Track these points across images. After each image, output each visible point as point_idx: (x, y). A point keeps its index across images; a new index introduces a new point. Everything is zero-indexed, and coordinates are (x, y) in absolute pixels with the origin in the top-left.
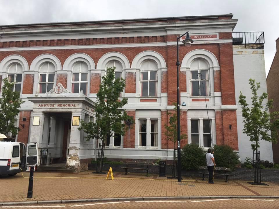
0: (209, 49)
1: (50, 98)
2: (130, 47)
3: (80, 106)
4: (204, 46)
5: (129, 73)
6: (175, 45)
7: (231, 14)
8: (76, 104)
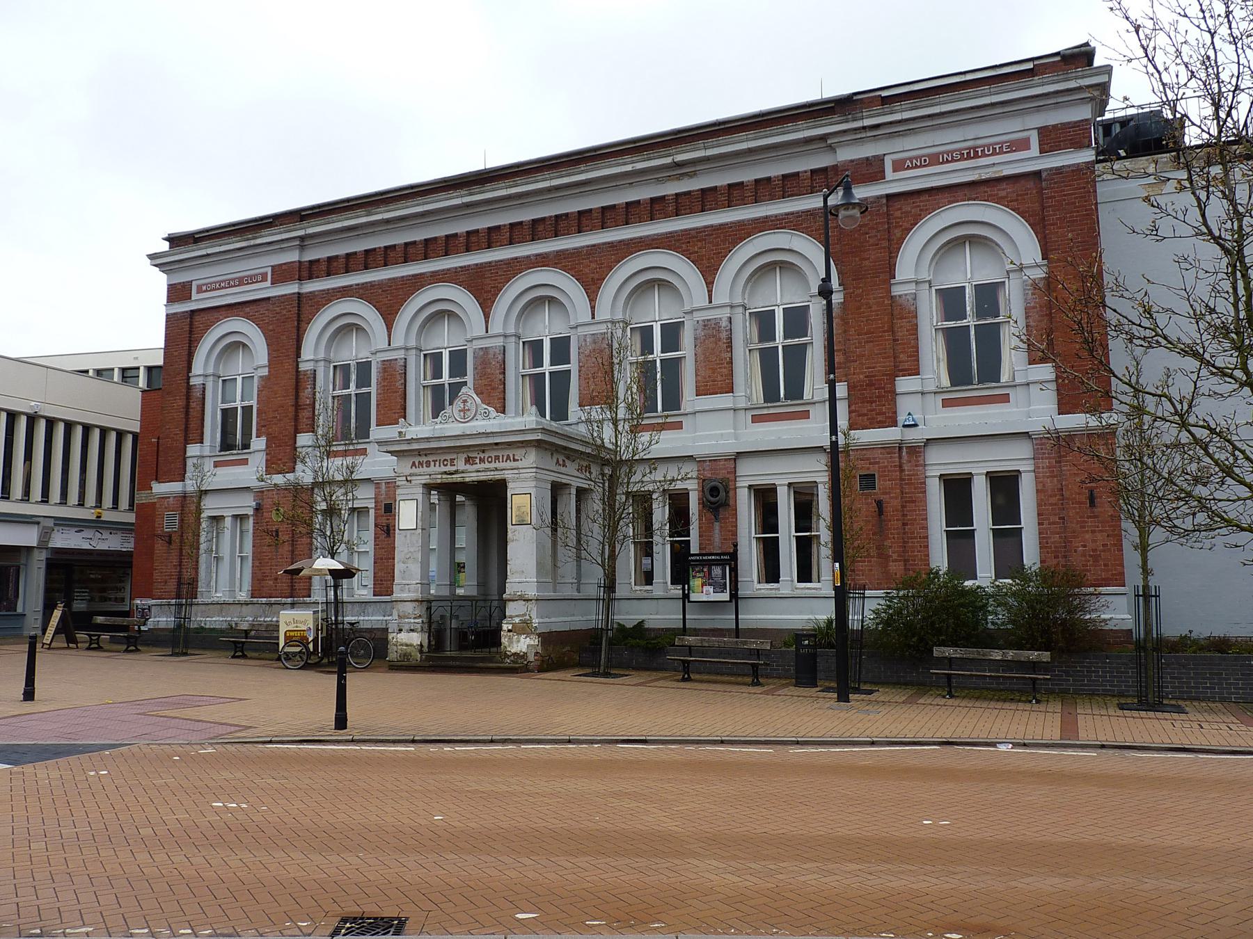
0: (1003, 198)
1: (439, 438)
2: (706, 227)
3: (530, 459)
4: (983, 188)
5: (706, 324)
6: (815, 209)
7: (1087, 44)
8: (519, 453)
